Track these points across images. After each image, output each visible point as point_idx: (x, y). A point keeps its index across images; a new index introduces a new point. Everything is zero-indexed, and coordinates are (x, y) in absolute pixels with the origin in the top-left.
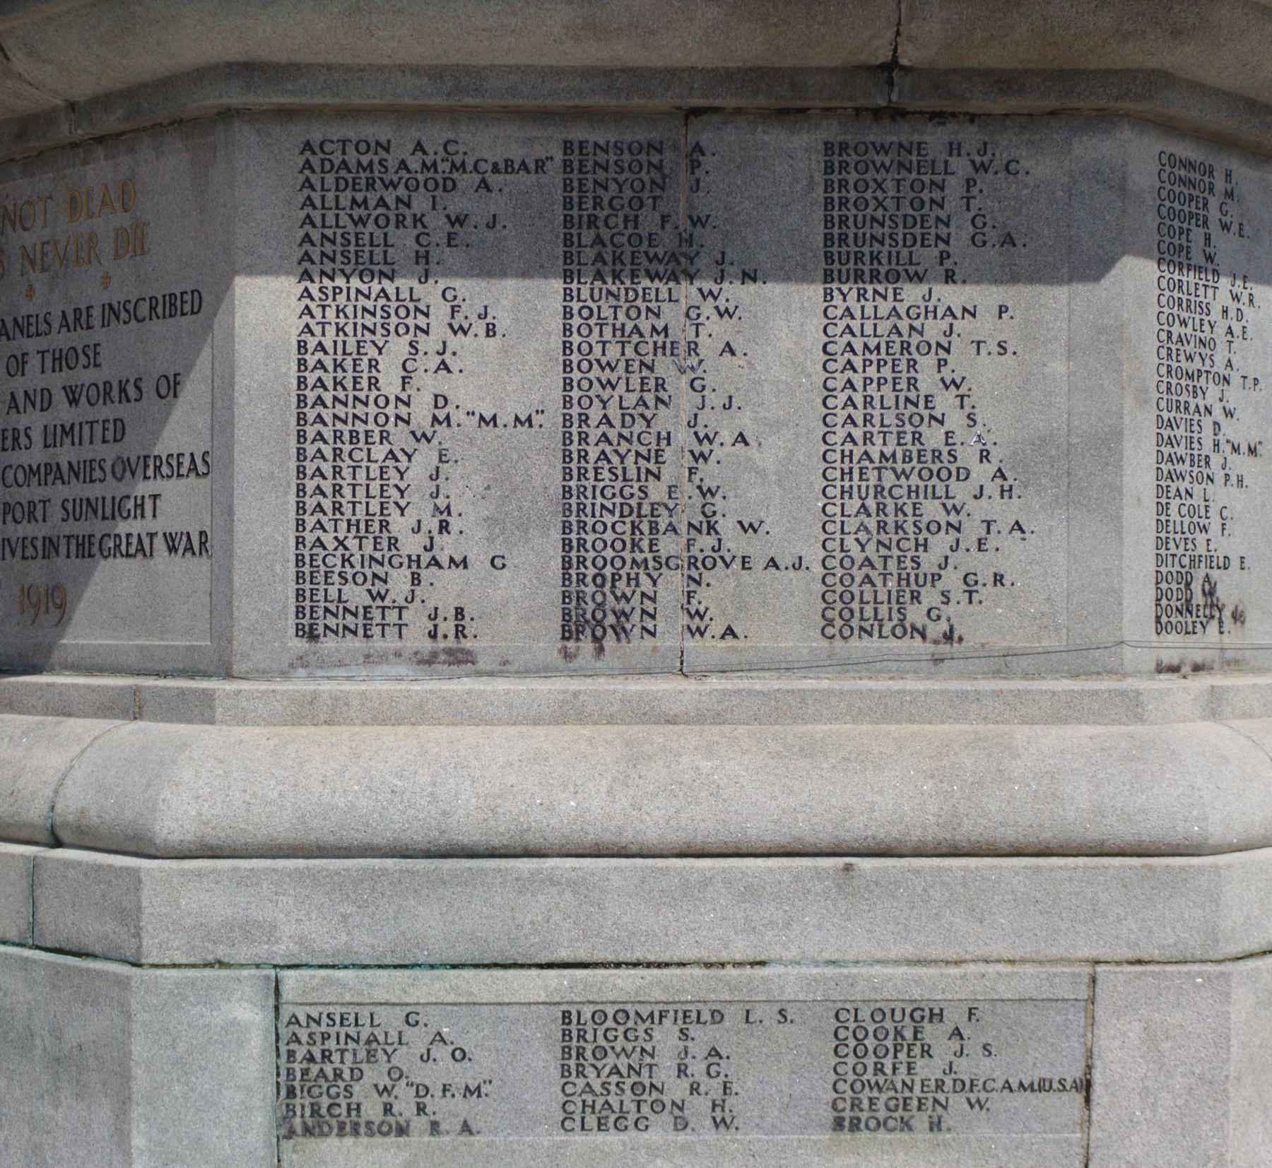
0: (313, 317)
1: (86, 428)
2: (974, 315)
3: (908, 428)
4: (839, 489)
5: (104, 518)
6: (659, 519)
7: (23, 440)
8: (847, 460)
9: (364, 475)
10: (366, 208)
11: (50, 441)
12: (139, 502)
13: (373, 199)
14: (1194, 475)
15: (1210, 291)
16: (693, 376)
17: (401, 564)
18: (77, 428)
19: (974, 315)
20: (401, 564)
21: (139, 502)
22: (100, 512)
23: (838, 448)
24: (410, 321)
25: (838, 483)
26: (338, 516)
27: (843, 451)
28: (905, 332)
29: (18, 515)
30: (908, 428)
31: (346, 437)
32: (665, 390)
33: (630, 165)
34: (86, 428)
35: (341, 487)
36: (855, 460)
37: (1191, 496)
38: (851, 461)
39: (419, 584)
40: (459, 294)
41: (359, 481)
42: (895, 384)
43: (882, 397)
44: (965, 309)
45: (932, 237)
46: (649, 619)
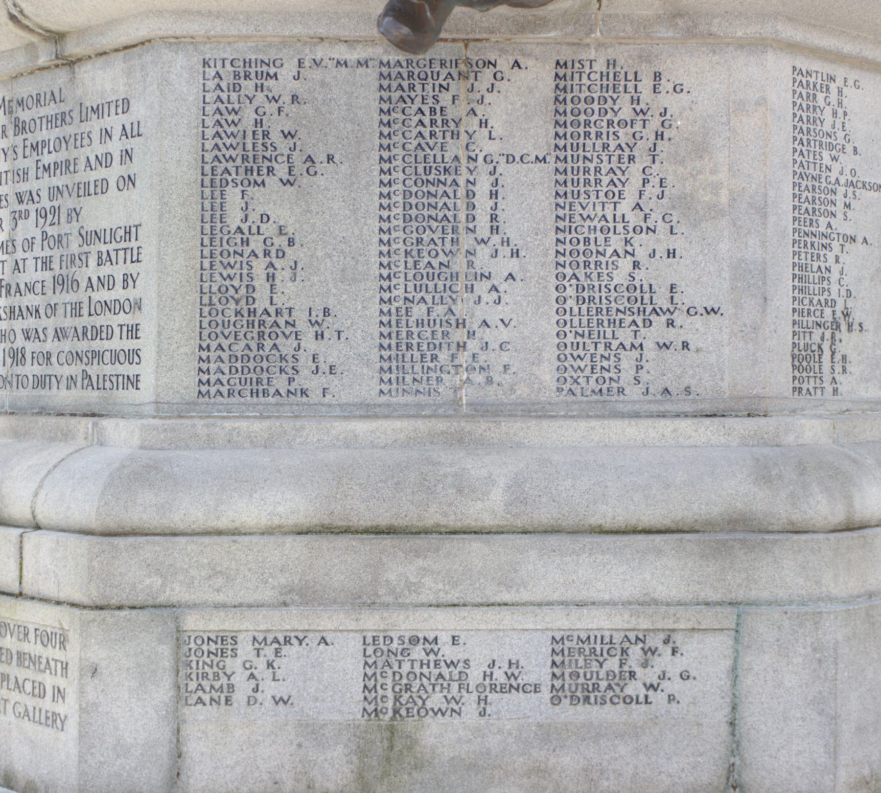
1: (106, 106)
2: (654, 232)
4: (599, 86)
5: (105, 243)
6: (459, 225)
7: (68, 119)
8: (604, 78)
10: (209, 374)
11: (84, 118)
12: (128, 230)
13: (214, 345)
14: (822, 211)
15: (807, 335)
16: (495, 71)
18: (100, 107)
19: (654, 232)
21: (128, 230)
22: (102, 240)
24: (205, 647)
25: (598, 83)
29: (52, 244)
34: (106, 106)
39: (233, 691)
43: (596, 238)
45: (599, 368)
46: (393, 656)
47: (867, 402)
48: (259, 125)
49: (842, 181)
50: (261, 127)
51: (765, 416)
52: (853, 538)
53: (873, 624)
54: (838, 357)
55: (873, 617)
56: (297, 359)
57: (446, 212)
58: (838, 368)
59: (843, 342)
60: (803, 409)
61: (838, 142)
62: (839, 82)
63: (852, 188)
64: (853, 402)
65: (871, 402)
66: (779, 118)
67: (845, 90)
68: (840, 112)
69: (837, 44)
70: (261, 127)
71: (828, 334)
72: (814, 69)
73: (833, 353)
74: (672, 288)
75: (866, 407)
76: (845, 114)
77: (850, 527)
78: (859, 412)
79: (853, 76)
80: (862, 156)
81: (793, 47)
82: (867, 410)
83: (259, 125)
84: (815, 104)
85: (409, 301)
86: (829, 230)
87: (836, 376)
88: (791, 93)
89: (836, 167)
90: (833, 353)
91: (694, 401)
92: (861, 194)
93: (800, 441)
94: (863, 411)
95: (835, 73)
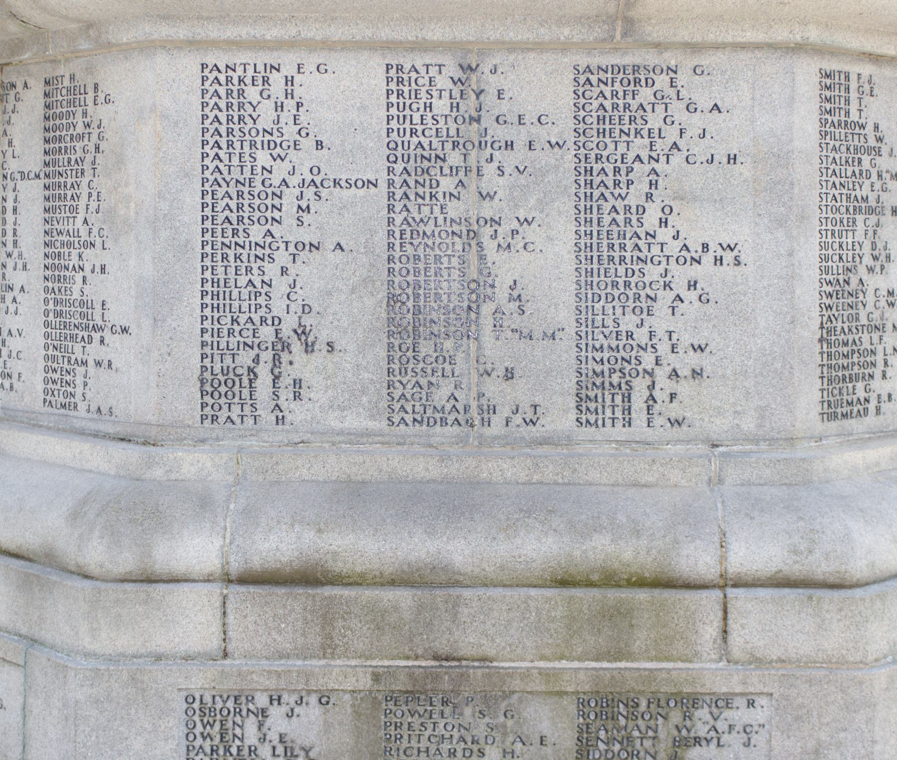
0: (221, 161)
3: (247, 137)
9: (233, 272)
17: (267, 348)
20: (267, 348)
23: (594, 114)
26: (231, 150)
27: (598, 130)
28: (235, 222)
30: (247, 137)
31: (236, 119)
32: (633, 339)
33: (259, 207)
35: (244, 104)
36: (594, 200)
37: (83, 270)
38: (591, 200)
40: (525, 253)
41: (233, 163)
42: (213, 257)
44: (227, 66)
47: (341, 433)
48: (428, 109)
49: (294, 181)
50: (431, 110)
51: (154, 445)
52: (125, 592)
53: (144, 690)
54: (286, 381)
55: (142, 682)
56: (577, 309)
57: (604, 178)
58: (285, 395)
59: (296, 365)
60: (217, 439)
61: (284, 138)
62: (288, 69)
63: (313, 189)
64: (312, 433)
65: (349, 434)
66: (176, 124)
67: (298, 78)
68: (290, 104)
69: (252, 32)
70: (431, 110)
71: (266, 356)
72: (238, 62)
73: (276, 378)
74: (103, 305)
75: (339, 439)
76: (299, 105)
77: (150, 579)
78: (327, 445)
79: (311, 61)
80: (333, 150)
81: (193, 44)
82: (340, 442)
83: (428, 109)
84: (242, 99)
85: (642, 261)
86: (269, 239)
87: (282, 402)
88: (200, 93)
89: (280, 171)
90: (276, 378)
91: (114, 422)
92: (331, 193)
93: (173, 476)
94: (334, 444)
95: (280, 61)
